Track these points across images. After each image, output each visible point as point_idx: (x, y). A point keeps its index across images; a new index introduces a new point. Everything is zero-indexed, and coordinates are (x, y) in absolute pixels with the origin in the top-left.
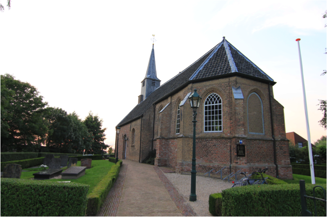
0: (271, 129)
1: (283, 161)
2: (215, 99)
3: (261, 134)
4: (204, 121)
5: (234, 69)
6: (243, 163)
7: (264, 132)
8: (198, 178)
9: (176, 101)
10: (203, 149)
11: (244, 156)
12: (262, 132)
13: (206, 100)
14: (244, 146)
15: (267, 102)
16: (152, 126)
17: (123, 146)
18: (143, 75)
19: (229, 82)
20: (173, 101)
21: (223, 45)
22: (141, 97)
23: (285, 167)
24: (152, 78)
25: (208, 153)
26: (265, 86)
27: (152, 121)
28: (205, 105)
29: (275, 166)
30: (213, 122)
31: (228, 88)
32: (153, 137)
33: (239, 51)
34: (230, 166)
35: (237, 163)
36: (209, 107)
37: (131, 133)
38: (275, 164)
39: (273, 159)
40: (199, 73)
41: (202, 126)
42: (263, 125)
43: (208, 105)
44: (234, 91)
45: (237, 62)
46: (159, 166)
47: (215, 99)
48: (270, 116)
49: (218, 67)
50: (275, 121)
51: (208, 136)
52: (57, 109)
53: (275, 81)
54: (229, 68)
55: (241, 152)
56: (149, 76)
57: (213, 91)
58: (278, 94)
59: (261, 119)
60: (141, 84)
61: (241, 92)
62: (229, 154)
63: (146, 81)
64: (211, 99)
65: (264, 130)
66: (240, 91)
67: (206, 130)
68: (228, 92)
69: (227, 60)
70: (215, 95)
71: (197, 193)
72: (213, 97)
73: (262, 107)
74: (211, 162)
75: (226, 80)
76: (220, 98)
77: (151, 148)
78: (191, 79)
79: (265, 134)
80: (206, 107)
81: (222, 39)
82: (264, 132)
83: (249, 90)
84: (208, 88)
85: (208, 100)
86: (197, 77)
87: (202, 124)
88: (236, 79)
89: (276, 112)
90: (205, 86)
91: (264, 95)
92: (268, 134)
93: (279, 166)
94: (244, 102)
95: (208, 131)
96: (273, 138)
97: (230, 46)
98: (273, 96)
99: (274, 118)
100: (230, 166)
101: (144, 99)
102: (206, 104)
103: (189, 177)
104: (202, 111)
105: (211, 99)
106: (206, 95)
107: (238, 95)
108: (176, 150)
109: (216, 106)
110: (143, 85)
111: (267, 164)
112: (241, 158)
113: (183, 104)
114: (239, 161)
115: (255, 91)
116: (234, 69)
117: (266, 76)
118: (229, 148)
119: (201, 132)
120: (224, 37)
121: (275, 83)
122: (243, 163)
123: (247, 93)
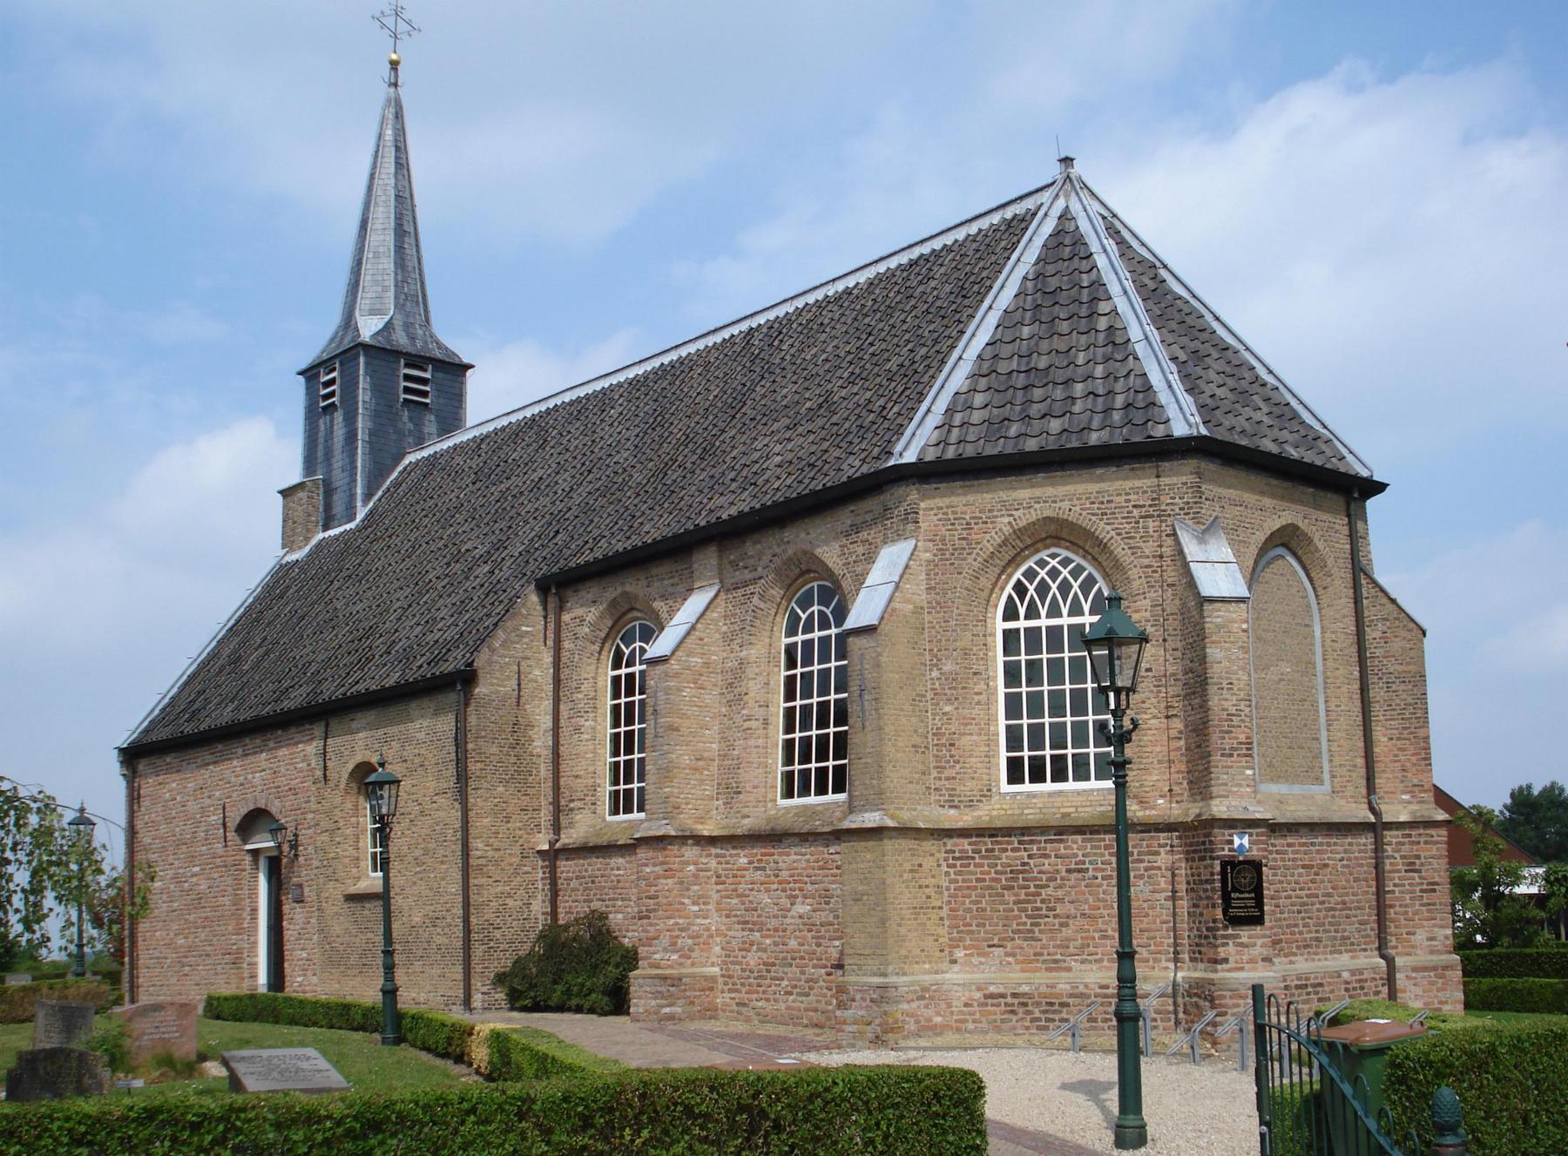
1: (1420, 937)
2: (1065, 588)
3: (1316, 788)
4: (1002, 723)
6: (1251, 961)
7: (1326, 776)
8: (1152, 1072)
10: (1009, 897)
11: (1258, 920)
12: (1319, 780)
13: (1009, 589)
14: (1256, 866)
16: (541, 743)
23: (1434, 968)
24: (401, 339)
25: (1036, 916)
27: (540, 713)
28: (1001, 626)
30: (823, 723)
31: (1151, 524)
32: (557, 828)
34: (1175, 984)
38: (1382, 956)
39: (1371, 929)
40: (950, 411)
41: (990, 756)
42: (1324, 734)
43: (1022, 624)
47: (1065, 588)
50: (1377, 710)
51: (1031, 816)
53: (466, 360)
54: (1145, 401)
55: (1242, 899)
59: (1314, 704)
61: (1227, 553)
62: (1166, 915)
64: (1043, 589)
65: (1326, 768)
67: (1015, 775)
72: (1054, 573)
73: (1318, 633)
74: (1055, 966)
77: (539, 906)
80: (1011, 636)
82: (1326, 776)
83: (1261, 537)
84: (1024, 518)
85: (1020, 589)
86: (942, 443)
87: (991, 742)
91: (1330, 562)
92: (1350, 790)
93: (1399, 961)
95: (1027, 787)
96: (1372, 809)
99: (1377, 693)
100: (1175, 984)
102: (1010, 614)
104: (986, 659)
105: (1043, 589)
106: (1014, 562)
107: (1218, 571)
108: (802, 908)
111: (1345, 957)
112: (1245, 933)
114: (1231, 948)
118: (1163, 883)
119: (988, 792)
123: (1253, 551)
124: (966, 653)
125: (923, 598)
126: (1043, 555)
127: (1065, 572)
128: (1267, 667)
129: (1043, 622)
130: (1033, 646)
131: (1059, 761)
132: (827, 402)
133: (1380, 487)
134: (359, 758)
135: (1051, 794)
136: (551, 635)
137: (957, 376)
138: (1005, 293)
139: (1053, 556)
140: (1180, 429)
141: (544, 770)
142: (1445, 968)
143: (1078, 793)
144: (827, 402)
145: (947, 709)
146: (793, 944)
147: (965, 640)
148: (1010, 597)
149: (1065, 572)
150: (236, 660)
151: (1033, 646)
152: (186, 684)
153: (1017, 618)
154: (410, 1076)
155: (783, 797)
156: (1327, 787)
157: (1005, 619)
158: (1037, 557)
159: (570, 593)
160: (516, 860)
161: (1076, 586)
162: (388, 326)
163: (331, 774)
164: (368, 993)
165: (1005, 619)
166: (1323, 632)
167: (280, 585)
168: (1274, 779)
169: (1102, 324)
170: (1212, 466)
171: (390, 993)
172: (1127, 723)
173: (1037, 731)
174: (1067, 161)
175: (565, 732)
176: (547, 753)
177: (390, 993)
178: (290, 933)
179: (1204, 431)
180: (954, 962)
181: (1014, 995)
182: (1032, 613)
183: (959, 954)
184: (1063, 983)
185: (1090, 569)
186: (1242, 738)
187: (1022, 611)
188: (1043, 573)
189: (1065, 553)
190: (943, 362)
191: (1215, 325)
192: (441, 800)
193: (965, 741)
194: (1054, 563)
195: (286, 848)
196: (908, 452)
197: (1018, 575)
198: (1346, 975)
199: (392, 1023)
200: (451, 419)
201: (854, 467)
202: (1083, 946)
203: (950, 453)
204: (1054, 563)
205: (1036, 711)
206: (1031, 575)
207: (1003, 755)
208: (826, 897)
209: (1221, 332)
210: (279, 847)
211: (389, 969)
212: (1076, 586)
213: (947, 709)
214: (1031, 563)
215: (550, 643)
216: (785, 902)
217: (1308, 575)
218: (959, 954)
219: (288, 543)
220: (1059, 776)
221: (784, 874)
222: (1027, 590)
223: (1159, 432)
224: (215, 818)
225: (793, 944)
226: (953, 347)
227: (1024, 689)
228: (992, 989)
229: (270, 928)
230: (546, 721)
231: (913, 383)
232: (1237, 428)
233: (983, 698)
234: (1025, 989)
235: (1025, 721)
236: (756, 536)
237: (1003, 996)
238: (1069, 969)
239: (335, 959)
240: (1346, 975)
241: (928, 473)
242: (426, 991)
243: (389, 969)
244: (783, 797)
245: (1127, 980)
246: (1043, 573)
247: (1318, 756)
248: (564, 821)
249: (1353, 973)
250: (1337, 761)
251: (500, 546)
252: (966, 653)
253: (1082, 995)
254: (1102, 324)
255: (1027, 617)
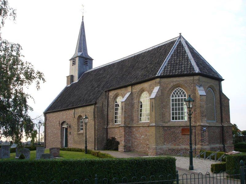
0: (220, 118)
1: (228, 142)
2: (180, 93)
5: (197, 70)
6: (206, 145)
7: (216, 120)
8: (194, 159)
9: (139, 92)
10: (172, 135)
12: (215, 120)
15: (218, 96)
17: (61, 134)
18: (72, 50)
19: (194, 80)
20: (134, 91)
21: (180, 41)
22: (71, 78)
23: (230, 146)
24: (84, 56)
26: (217, 82)
29: (223, 145)
33: (194, 48)
35: (202, 145)
36: (176, 99)
37: (76, 120)
40: (165, 68)
41: (170, 116)
44: (197, 88)
45: (197, 61)
46: (124, 151)
47: (180, 93)
48: (220, 107)
49: (182, 65)
51: (175, 125)
52: (244, 131)
54: (192, 67)
56: (80, 54)
57: (179, 86)
58: (227, 89)
59: (214, 110)
60: (68, 63)
63: (77, 59)
64: (177, 93)
66: (202, 88)
67: (173, 119)
68: (192, 88)
69: (188, 59)
70: (180, 90)
71: (194, 165)
72: (179, 91)
73: (215, 100)
74: (178, 145)
75: (191, 78)
76: (185, 93)
77: (105, 135)
78: (159, 75)
79: (215, 123)
80: (173, 100)
81: (179, 35)
83: (207, 87)
84: (175, 83)
85: (174, 93)
86: (164, 73)
87: (170, 114)
88: (199, 78)
89: (223, 103)
90: (173, 82)
93: (225, 145)
94: (206, 98)
95: (175, 120)
97: (187, 43)
98: (222, 90)
100: (195, 148)
101: (76, 80)
102: (173, 97)
103: (188, 159)
104: (170, 103)
105: (177, 93)
106: (173, 89)
108: (143, 137)
109: (179, 99)
110: (74, 63)
113: (154, 97)
115: (210, 87)
116: (197, 70)
117: (216, 73)
119: (169, 121)
120: (180, 34)
121: (223, 80)
122: (206, 145)
124: (167, 102)
125: (160, 94)
126: (177, 89)
127: (180, 91)
128: (208, 105)
129: (177, 98)
130: (176, 101)
131: (179, 117)
132: (146, 67)
133: (223, 80)
134: (79, 114)
135: (178, 121)
136: (107, 98)
137: (165, 63)
138: (172, 52)
139: (179, 89)
140: (197, 72)
141: (106, 117)
142: (232, 146)
143: (182, 121)
144: (146, 67)
145: (164, 109)
146: (141, 141)
147: (166, 100)
148: (173, 94)
149: (180, 91)
150: (60, 100)
151: (176, 101)
152: (53, 104)
153: (176, 97)
154: (89, 157)
155: (172, 120)
156: (216, 121)
157: (172, 97)
158: (177, 89)
159: (110, 92)
160: (102, 129)
161: (182, 93)
162: (82, 54)
163: (75, 117)
164: (83, 147)
165: (172, 97)
166: (215, 99)
167: (66, 90)
168: (209, 120)
169: (186, 57)
170: (201, 77)
171: (86, 147)
172: (191, 112)
173: (176, 113)
174: (180, 34)
175: (109, 111)
176: (106, 114)
177: (86, 147)
178: (69, 138)
179: (200, 72)
180: (164, 144)
181: (173, 149)
182: (179, 96)
183: (165, 143)
184: (179, 147)
185: (184, 91)
186: (205, 114)
187: (174, 96)
188: (177, 91)
189: (180, 88)
190: (163, 62)
191: (201, 57)
192: (91, 121)
193: (166, 114)
194: (179, 90)
195: (68, 127)
196: (158, 74)
197: (174, 91)
198: (218, 147)
199: (87, 151)
200: (91, 67)
201: (151, 76)
202: (182, 143)
203: (165, 74)
204: (179, 90)
205: (176, 110)
206: (175, 91)
207: (171, 116)
208: (146, 135)
209: (201, 58)
210: (67, 127)
211: (86, 144)
212: (182, 93)
213: (164, 109)
214: (176, 90)
215: (107, 99)
216: (140, 136)
217: (214, 92)
218: (165, 143)
219: (68, 84)
220: (179, 119)
221: (140, 132)
222: (175, 93)
223: (194, 72)
224: (58, 123)
225: (141, 141)
226: (165, 59)
227: (177, 107)
228: (170, 148)
229: (65, 138)
230: (106, 110)
231: (159, 64)
232: (206, 72)
233: (169, 108)
234: (174, 148)
235: (174, 112)
236: (137, 85)
237: (171, 149)
238: (180, 146)
239: (75, 142)
240: (218, 147)
241: (161, 77)
242: (90, 147)
243: (86, 144)
244: (172, 120)
245: (191, 147)
246: (177, 91)
247: (215, 117)
248: (109, 124)
249: (219, 147)
250: (217, 118)
251: (99, 85)
252: (167, 102)
253: (182, 149)
254: (186, 57)
255: (181, 97)
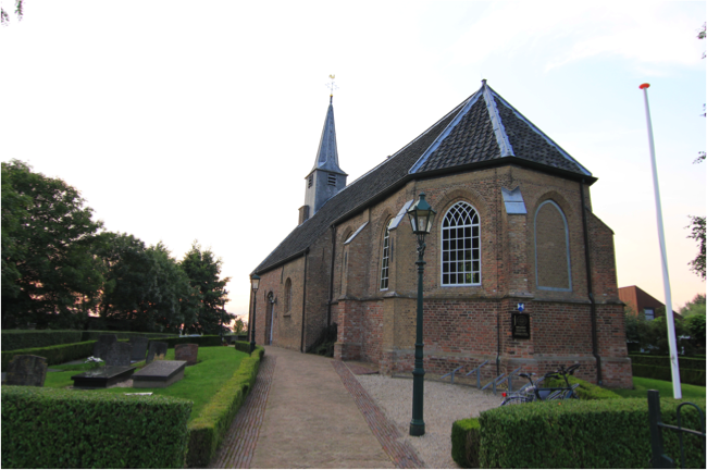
0: (585, 280)
1: (612, 349)
2: (464, 215)
3: (565, 290)
4: (442, 262)
5: (505, 149)
6: (524, 354)
7: (570, 285)
8: (427, 386)
9: (381, 220)
10: (440, 323)
11: (528, 337)
12: (567, 287)
13: (445, 216)
14: (527, 316)
15: (578, 222)
16: (329, 272)
17: (267, 317)
18: (309, 162)
19: (496, 177)
20: (374, 218)
21: (481, 97)
22: (305, 210)
23: (617, 363)
24: (328, 168)
25: (449, 331)
26: (573, 186)
27: (329, 262)
28: (443, 228)
29: (595, 359)
30: (460, 264)
31: (493, 190)
32: (331, 298)
33: (516, 111)
34: (498, 361)
35: (513, 353)
36: (453, 231)
37: (283, 287)
38: (596, 356)
39: (589, 345)
40: (430, 158)
41: (437, 274)
42: (569, 270)
43: (449, 228)
44: (505, 197)
45: (512, 134)
46: (343, 359)
47: (464, 215)
48: (583, 252)
49: (471, 145)
50: (594, 262)
51: (449, 294)
53: (594, 176)
54: (495, 148)
55: (521, 329)
56: (322, 164)
57: (461, 198)
58: (602, 203)
59: (565, 258)
60: (304, 183)
61: (520, 199)
62: (495, 333)
63: (315, 175)
64: (457, 216)
65: (570, 282)
66: (518, 197)
67: (445, 281)
68: (492, 198)
69: (490, 131)
70: (465, 206)
71: (426, 418)
72: (461, 210)
73: (567, 232)
74: (455, 350)
75: (490, 173)
76: (477, 212)
77: (326, 321)
78: (414, 172)
80: (445, 232)
81: (479, 85)
82: (570, 285)
83: (539, 195)
84: (449, 190)
85: (449, 216)
86: (425, 167)
87: (437, 269)
88: (511, 171)
89: (596, 242)
90: (444, 187)
91: (572, 206)
92: (580, 291)
93: (602, 359)
94: (527, 222)
95: (450, 285)
96: (591, 299)
97: (498, 100)
98: (590, 207)
99: (593, 255)
100: (498, 361)
101: (312, 214)
102: (446, 224)
103: (409, 384)
104: (437, 240)
105: (457, 216)
106: (446, 206)
107: (514, 205)
108: (381, 325)
109: (468, 230)
110: (310, 185)
111: (577, 355)
112: (522, 343)
113: (395, 226)
114: (516, 348)
115: (552, 196)
116: (505, 149)
117: (575, 164)
118: (495, 321)
119: (436, 286)
120: (484, 81)
121: (595, 180)
122: (524, 354)
123: (533, 202)
